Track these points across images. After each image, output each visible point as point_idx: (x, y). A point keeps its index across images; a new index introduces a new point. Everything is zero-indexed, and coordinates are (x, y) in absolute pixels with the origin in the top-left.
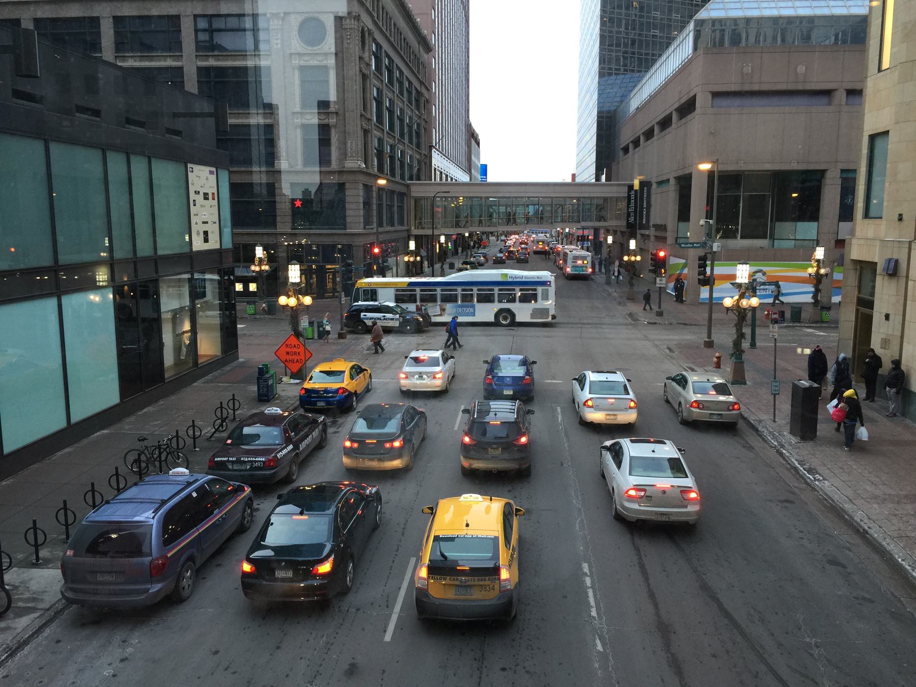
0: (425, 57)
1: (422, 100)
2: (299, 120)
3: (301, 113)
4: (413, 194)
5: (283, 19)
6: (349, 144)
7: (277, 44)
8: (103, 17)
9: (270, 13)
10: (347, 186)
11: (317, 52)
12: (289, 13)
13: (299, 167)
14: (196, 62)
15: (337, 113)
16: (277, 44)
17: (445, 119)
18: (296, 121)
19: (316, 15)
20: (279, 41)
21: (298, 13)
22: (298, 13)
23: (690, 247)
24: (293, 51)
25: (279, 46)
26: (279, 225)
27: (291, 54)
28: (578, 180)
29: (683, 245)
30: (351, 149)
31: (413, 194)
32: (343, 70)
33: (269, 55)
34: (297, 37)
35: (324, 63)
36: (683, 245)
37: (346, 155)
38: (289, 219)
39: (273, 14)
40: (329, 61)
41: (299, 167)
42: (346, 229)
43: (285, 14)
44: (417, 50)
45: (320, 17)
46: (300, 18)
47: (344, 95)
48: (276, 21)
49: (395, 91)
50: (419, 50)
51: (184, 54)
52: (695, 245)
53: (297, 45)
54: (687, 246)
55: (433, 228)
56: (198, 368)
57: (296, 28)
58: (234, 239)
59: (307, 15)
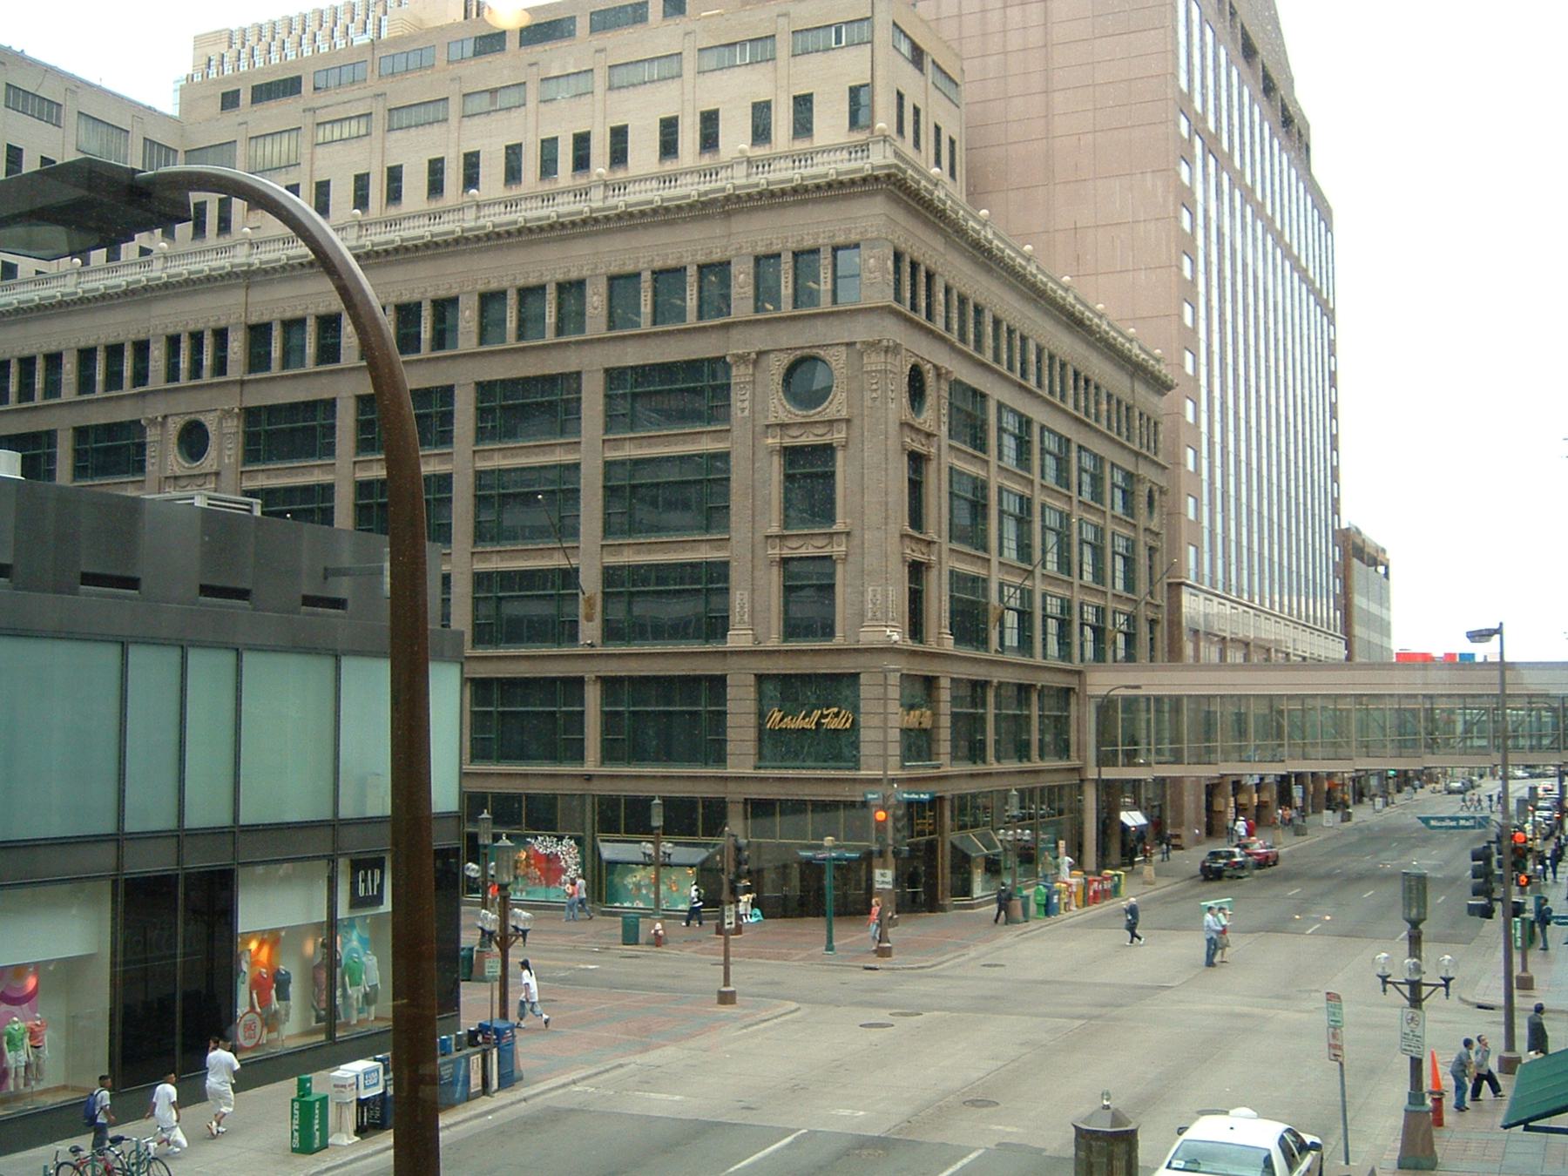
0: (1158, 405)
1: (1142, 492)
2: (777, 551)
3: (782, 537)
4: (1091, 691)
5: (756, 363)
6: (869, 596)
7: (743, 410)
8: (460, 386)
9: (864, 342)
10: (863, 679)
11: (817, 418)
13: (774, 641)
14: (603, 452)
16: (743, 410)
17: (1313, 530)
19: (815, 351)
20: (746, 404)
21: (781, 350)
22: (781, 350)
23: (1453, 827)
24: (772, 420)
25: (746, 413)
26: (730, 760)
28: (1489, 660)
29: (1433, 823)
31: (1091, 691)
33: (728, 431)
34: (781, 394)
35: (826, 440)
36: (1433, 823)
37: (862, 615)
38: (750, 747)
39: (737, 356)
41: (774, 641)
42: (859, 769)
43: (760, 354)
46: (786, 360)
48: (742, 368)
51: (583, 439)
52: (1462, 822)
53: (779, 408)
54: (1444, 824)
56: (336, 1043)
57: (778, 379)
58: (464, 784)
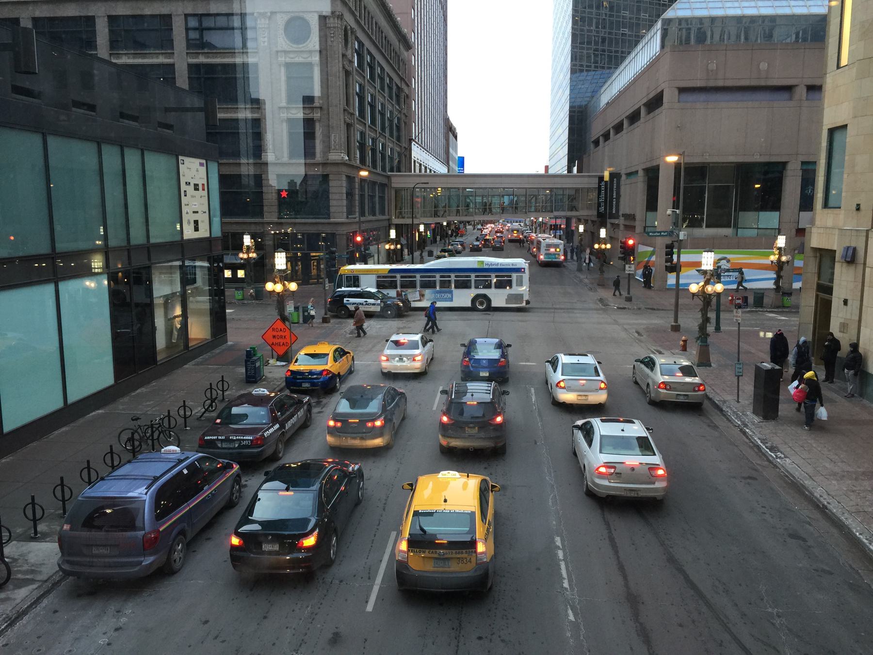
0: (405, 54)
1: (402, 95)
2: (285, 115)
3: (287, 108)
4: (394, 185)
5: (270, 18)
6: (332, 138)
7: (264, 42)
8: (98, 17)
9: (258, 12)
10: (331, 177)
11: (302, 49)
12: (276, 12)
13: (285, 159)
14: (187, 59)
15: (321, 108)
16: (264, 42)
17: (424, 113)
18: (282, 115)
19: (301, 14)
20: (266, 39)
21: (284, 12)
22: (284, 12)
23: (658, 236)
24: (280, 49)
25: (266, 44)
26: (265, 214)
27: (277, 52)
28: (551, 171)
29: (650, 234)
30: (335, 142)
31: (394, 185)
32: (327, 67)
33: (257, 52)
34: (284, 35)
35: (309, 60)
36: (650, 234)
37: (330, 147)
38: (275, 209)
39: (260, 13)
40: (313, 59)
41: (285, 159)
42: (330, 219)
43: (272, 13)
44: (398, 48)
45: (305, 16)
46: (286, 18)
47: (328, 91)
48: (263, 20)
49: (377, 86)
50: (400, 48)
51: (175, 52)
52: (662, 234)
53: (283, 43)
54: (655, 234)
55: (413, 218)
56: (189, 351)
57: (282, 27)
58: (223, 228)
59: (293, 15)
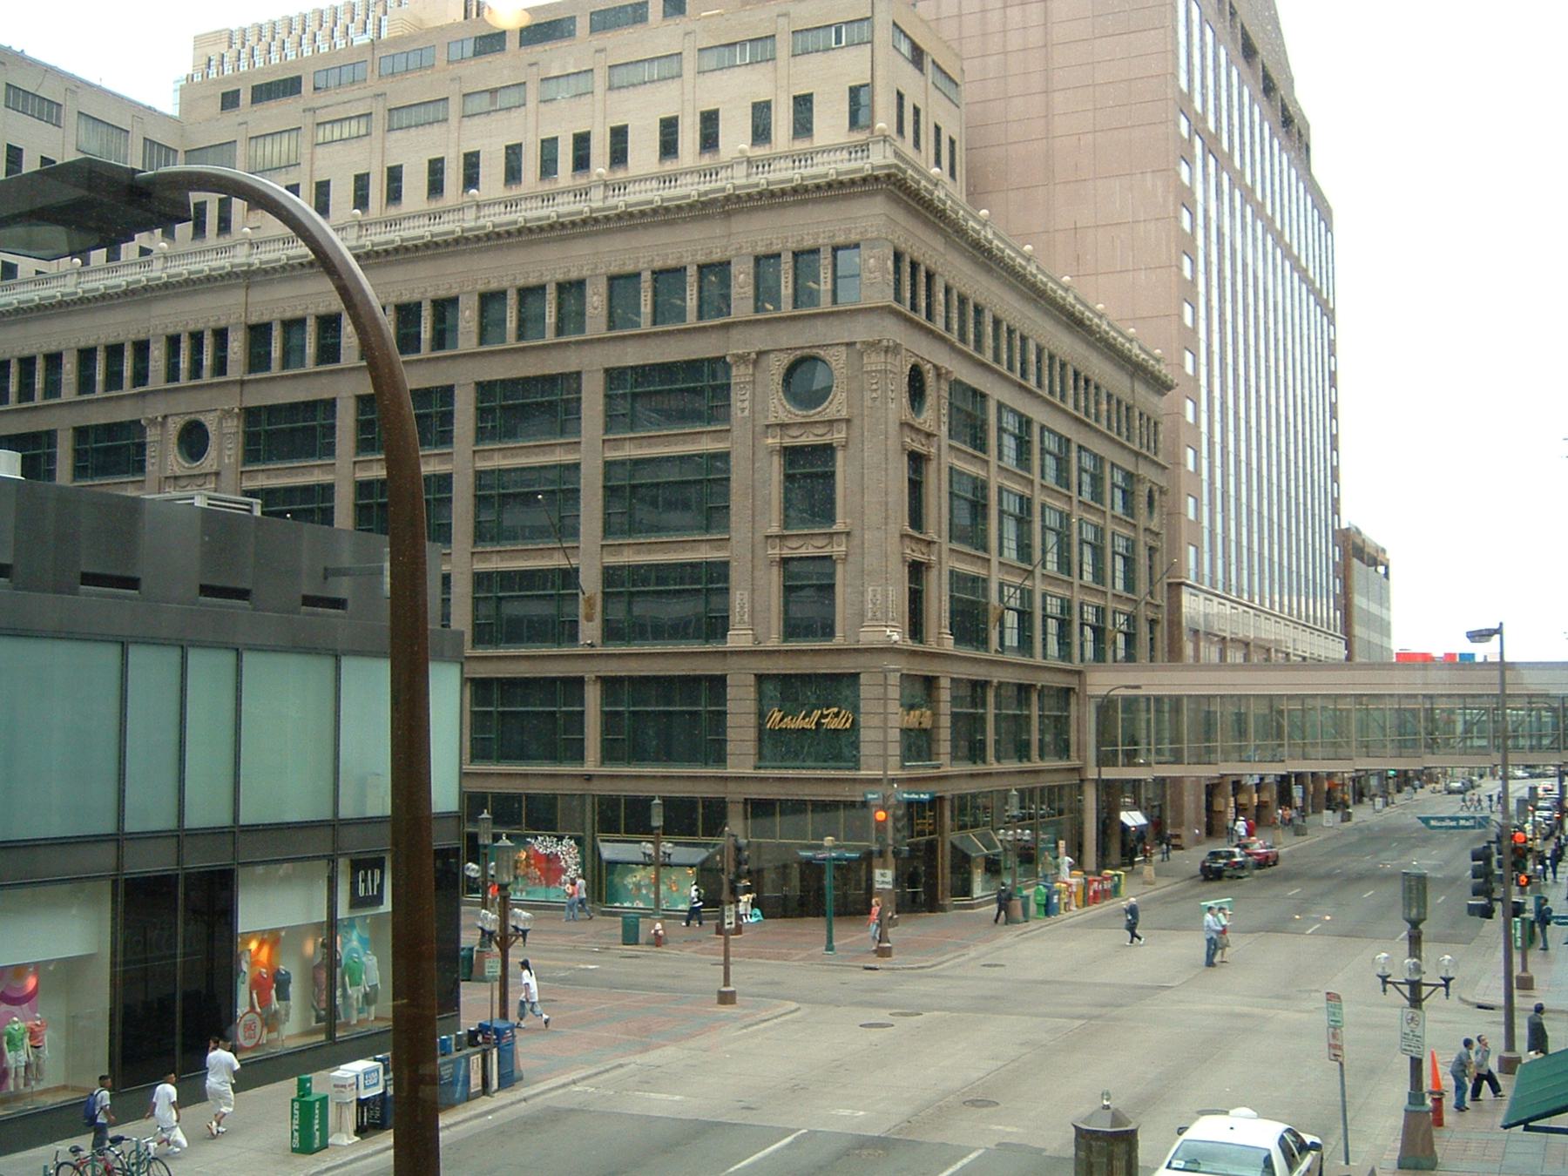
0: (1158, 405)
1: (1142, 492)
2: (777, 551)
3: (782, 537)
4: (1091, 691)
5: (756, 363)
6: (869, 596)
7: (743, 410)
8: (460, 386)
9: (864, 342)
10: (863, 679)
11: (817, 418)
13: (774, 641)
14: (603, 452)
16: (743, 410)
17: (1313, 530)
19: (815, 351)
20: (746, 404)
21: (781, 350)
22: (781, 350)
23: (1453, 827)
24: (772, 420)
25: (746, 413)
26: (730, 760)
28: (1489, 660)
29: (1433, 823)
31: (1091, 691)
33: (728, 431)
34: (781, 394)
35: (826, 440)
36: (1433, 823)
37: (862, 615)
38: (750, 747)
39: (737, 356)
41: (774, 641)
42: (859, 769)
43: (760, 354)
46: (786, 360)
48: (742, 368)
51: (583, 439)
52: (1462, 822)
53: (779, 408)
54: (1444, 824)
56: (336, 1043)
57: (778, 379)
58: (464, 784)
